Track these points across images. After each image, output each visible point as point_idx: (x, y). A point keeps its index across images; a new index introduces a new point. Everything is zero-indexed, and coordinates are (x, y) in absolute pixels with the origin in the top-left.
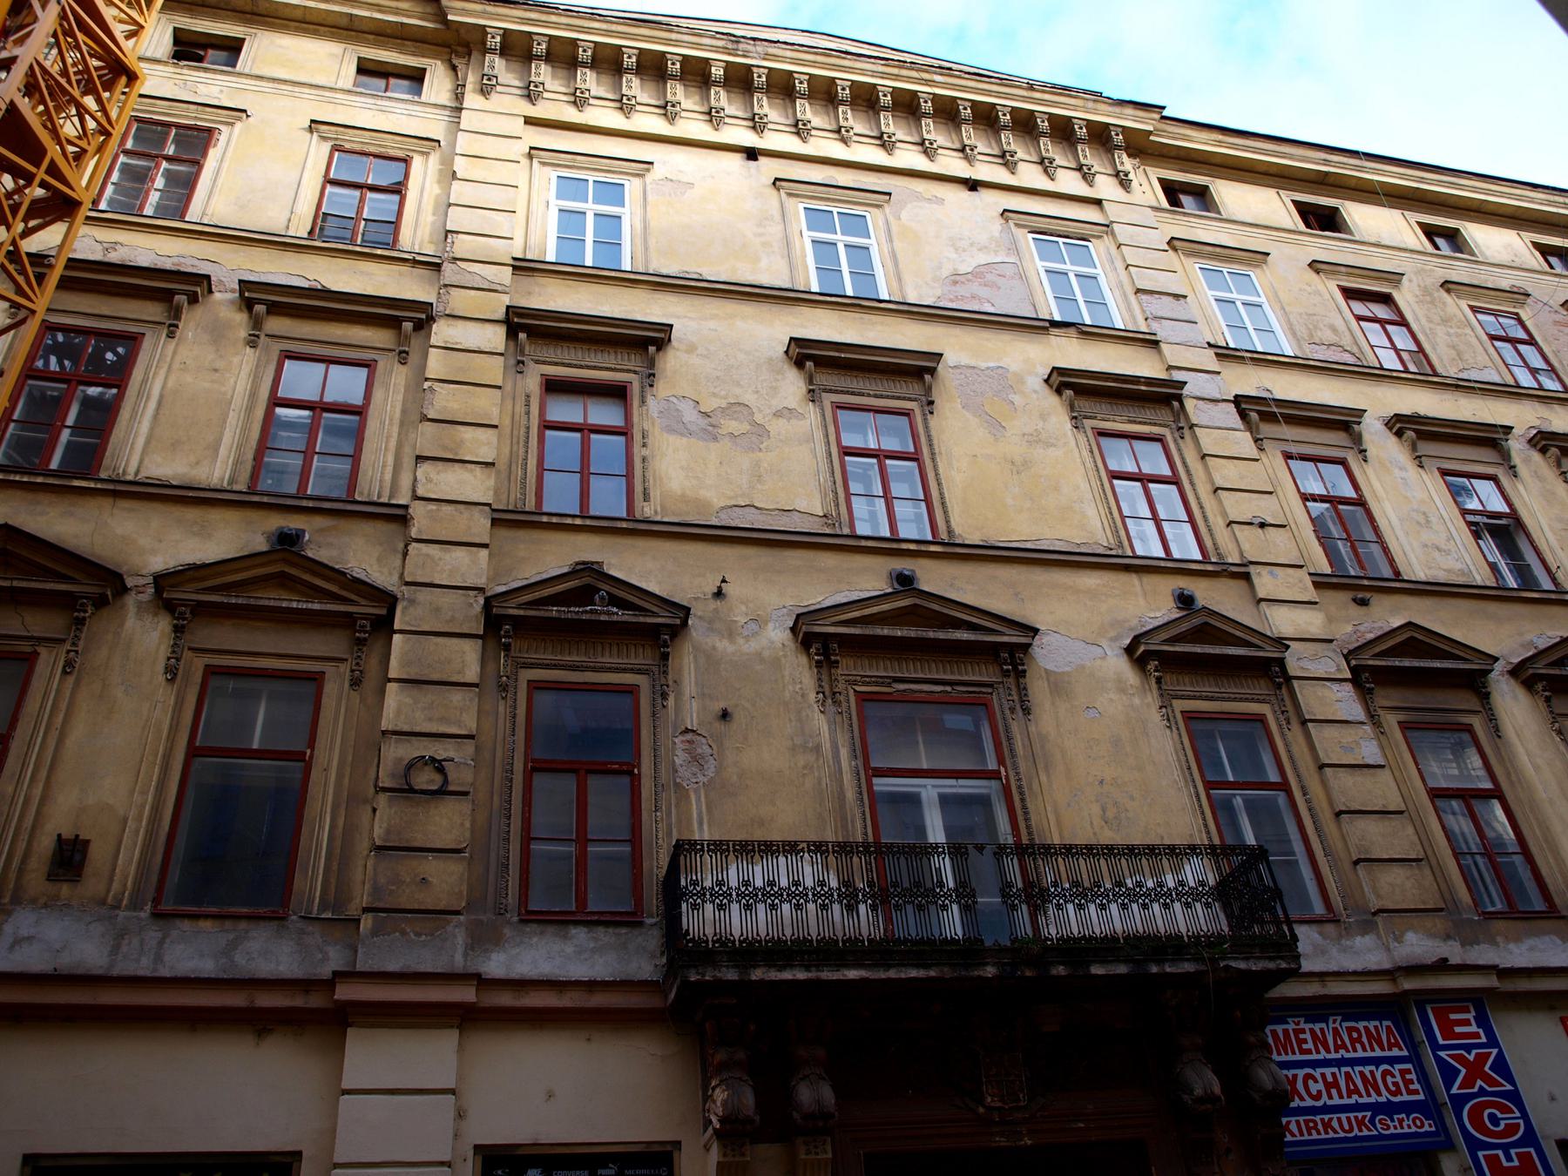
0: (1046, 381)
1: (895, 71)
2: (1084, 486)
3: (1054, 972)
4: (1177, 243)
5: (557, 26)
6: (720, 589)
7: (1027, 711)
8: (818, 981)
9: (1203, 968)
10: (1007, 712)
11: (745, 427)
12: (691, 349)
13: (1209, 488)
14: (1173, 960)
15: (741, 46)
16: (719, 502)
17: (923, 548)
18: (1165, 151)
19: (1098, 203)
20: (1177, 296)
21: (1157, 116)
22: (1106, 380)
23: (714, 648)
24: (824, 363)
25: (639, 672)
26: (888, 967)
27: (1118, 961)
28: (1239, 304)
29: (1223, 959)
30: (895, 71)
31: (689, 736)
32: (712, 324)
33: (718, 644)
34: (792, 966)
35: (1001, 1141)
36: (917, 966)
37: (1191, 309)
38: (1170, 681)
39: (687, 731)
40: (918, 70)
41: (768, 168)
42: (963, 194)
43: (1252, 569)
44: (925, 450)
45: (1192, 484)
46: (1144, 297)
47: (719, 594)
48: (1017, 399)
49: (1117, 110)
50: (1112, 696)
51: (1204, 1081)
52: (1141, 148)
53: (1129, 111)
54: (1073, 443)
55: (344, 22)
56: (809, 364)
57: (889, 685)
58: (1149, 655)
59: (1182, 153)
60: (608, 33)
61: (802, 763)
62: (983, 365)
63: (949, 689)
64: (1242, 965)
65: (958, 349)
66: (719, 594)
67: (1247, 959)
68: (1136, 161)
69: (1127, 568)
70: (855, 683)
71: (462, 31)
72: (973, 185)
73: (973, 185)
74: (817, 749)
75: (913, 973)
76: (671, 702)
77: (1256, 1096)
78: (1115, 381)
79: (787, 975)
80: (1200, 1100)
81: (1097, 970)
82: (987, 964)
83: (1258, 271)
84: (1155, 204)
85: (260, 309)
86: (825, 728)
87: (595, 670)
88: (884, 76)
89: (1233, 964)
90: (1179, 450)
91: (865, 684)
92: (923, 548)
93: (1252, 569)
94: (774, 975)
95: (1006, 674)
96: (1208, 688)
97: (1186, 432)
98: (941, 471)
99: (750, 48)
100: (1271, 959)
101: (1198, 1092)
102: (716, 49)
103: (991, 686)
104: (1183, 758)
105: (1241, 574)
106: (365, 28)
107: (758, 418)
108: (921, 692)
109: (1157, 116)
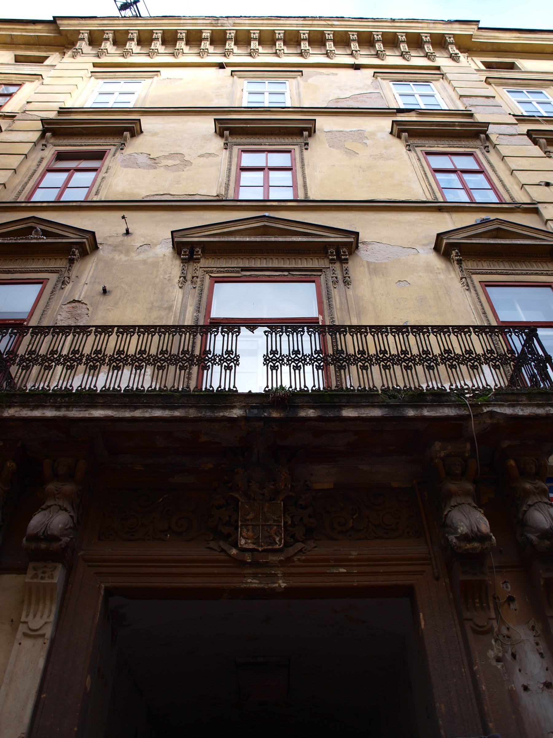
0: (391, 133)
1: (310, 22)
2: (412, 176)
3: (303, 414)
4: (489, 80)
5: (118, 25)
6: (127, 230)
7: (347, 283)
8: (64, 419)
9: (466, 412)
10: (330, 284)
11: (178, 162)
12: (155, 134)
13: (508, 173)
14: (430, 406)
15: (220, 22)
16: (143, 196)
17: (283, 204)
18: (484, 47)
19: (438, 68)
20: (487, 97)
21: (475, 27)
22: (431, 125)
23: (113, 259)
24: (234, 132)
25: (52, 272)
26: (136, 408)
27: (373, 406)
28: (534, 103)
29: (487, 405)
30: (310, 22)
31: (74, 305)
32: (172, 125)
33: (117, 257)
34: (44, 407)
35: (253, 583)
36: (164, 408)
37: (498, 100)
38: (469, 265)
39: (74, 301)
40: (325, 20)
41: (229, 70)
42: (351, 72)
43: (539, 206)
44: (298, 165)
45: (494, 170)
46: (465, 99)
47: (128, 233)
48: (368, 142)
49: (449, 26)
50: (422, 274)
51: (470, 519)
52: (468, 46)
53: (457, 26)
54: (407, 157)
55: (8, 40)
56: (227, 133)
57: (238, 272)
58: (451, 246)
59: (495, 47)
60: (145, 25)
61: (155, 316)
62: (348, 130)
63: (286, 273)
64: (508, 411)
65: (147, 123)
66: (128, 233)
67: (513, 406)
68: (466, 55)
69: (440, 209)
70: (212, 272)
71: (69, 35)
72: (357, 67)
73: (357, 67)
74: (170, 308)
75: (158, 413)
76: (68, 287)
77: (533, 537)
78: (437, 126)
79: (37, 413)
80: (465, 538)
81: (347, 413)
82: (233, 407)
83: (548, 90)
84: (477, 68)
85: (227, 133)
86: (181, 296)
87: (21, 272)
88: (303, 25)
89: (498, 410)
90: (486, 157)
91: (218, 272)
92: (283, 204)
93: (539, 206)
94: (26, 413)
95: (332, 261)
96: (505, 266)
97: (491, 149)
98: (307, 172)
99: (225, 22)
100: (539, 406)
101: (463, 529)
102: (206, 24)
103: (320, 270)
104: (479, 307)
105: (533, 209)
106: (19, 42)
107: (187, 158)
108: (265, 275)
109: (475, 27)
